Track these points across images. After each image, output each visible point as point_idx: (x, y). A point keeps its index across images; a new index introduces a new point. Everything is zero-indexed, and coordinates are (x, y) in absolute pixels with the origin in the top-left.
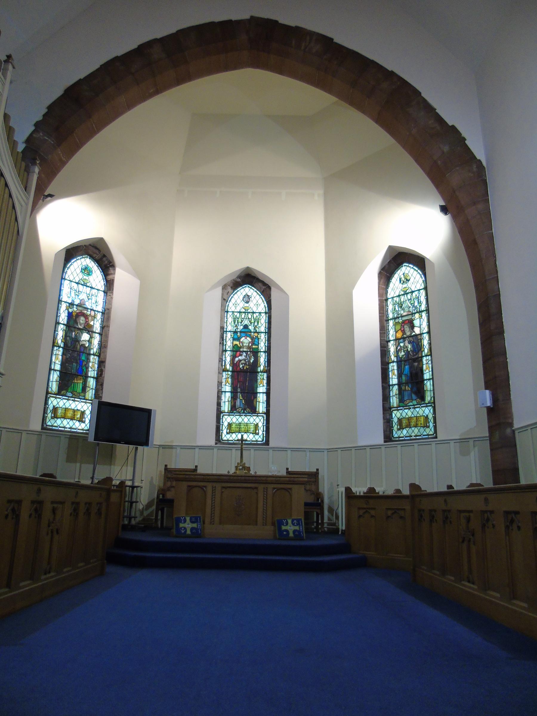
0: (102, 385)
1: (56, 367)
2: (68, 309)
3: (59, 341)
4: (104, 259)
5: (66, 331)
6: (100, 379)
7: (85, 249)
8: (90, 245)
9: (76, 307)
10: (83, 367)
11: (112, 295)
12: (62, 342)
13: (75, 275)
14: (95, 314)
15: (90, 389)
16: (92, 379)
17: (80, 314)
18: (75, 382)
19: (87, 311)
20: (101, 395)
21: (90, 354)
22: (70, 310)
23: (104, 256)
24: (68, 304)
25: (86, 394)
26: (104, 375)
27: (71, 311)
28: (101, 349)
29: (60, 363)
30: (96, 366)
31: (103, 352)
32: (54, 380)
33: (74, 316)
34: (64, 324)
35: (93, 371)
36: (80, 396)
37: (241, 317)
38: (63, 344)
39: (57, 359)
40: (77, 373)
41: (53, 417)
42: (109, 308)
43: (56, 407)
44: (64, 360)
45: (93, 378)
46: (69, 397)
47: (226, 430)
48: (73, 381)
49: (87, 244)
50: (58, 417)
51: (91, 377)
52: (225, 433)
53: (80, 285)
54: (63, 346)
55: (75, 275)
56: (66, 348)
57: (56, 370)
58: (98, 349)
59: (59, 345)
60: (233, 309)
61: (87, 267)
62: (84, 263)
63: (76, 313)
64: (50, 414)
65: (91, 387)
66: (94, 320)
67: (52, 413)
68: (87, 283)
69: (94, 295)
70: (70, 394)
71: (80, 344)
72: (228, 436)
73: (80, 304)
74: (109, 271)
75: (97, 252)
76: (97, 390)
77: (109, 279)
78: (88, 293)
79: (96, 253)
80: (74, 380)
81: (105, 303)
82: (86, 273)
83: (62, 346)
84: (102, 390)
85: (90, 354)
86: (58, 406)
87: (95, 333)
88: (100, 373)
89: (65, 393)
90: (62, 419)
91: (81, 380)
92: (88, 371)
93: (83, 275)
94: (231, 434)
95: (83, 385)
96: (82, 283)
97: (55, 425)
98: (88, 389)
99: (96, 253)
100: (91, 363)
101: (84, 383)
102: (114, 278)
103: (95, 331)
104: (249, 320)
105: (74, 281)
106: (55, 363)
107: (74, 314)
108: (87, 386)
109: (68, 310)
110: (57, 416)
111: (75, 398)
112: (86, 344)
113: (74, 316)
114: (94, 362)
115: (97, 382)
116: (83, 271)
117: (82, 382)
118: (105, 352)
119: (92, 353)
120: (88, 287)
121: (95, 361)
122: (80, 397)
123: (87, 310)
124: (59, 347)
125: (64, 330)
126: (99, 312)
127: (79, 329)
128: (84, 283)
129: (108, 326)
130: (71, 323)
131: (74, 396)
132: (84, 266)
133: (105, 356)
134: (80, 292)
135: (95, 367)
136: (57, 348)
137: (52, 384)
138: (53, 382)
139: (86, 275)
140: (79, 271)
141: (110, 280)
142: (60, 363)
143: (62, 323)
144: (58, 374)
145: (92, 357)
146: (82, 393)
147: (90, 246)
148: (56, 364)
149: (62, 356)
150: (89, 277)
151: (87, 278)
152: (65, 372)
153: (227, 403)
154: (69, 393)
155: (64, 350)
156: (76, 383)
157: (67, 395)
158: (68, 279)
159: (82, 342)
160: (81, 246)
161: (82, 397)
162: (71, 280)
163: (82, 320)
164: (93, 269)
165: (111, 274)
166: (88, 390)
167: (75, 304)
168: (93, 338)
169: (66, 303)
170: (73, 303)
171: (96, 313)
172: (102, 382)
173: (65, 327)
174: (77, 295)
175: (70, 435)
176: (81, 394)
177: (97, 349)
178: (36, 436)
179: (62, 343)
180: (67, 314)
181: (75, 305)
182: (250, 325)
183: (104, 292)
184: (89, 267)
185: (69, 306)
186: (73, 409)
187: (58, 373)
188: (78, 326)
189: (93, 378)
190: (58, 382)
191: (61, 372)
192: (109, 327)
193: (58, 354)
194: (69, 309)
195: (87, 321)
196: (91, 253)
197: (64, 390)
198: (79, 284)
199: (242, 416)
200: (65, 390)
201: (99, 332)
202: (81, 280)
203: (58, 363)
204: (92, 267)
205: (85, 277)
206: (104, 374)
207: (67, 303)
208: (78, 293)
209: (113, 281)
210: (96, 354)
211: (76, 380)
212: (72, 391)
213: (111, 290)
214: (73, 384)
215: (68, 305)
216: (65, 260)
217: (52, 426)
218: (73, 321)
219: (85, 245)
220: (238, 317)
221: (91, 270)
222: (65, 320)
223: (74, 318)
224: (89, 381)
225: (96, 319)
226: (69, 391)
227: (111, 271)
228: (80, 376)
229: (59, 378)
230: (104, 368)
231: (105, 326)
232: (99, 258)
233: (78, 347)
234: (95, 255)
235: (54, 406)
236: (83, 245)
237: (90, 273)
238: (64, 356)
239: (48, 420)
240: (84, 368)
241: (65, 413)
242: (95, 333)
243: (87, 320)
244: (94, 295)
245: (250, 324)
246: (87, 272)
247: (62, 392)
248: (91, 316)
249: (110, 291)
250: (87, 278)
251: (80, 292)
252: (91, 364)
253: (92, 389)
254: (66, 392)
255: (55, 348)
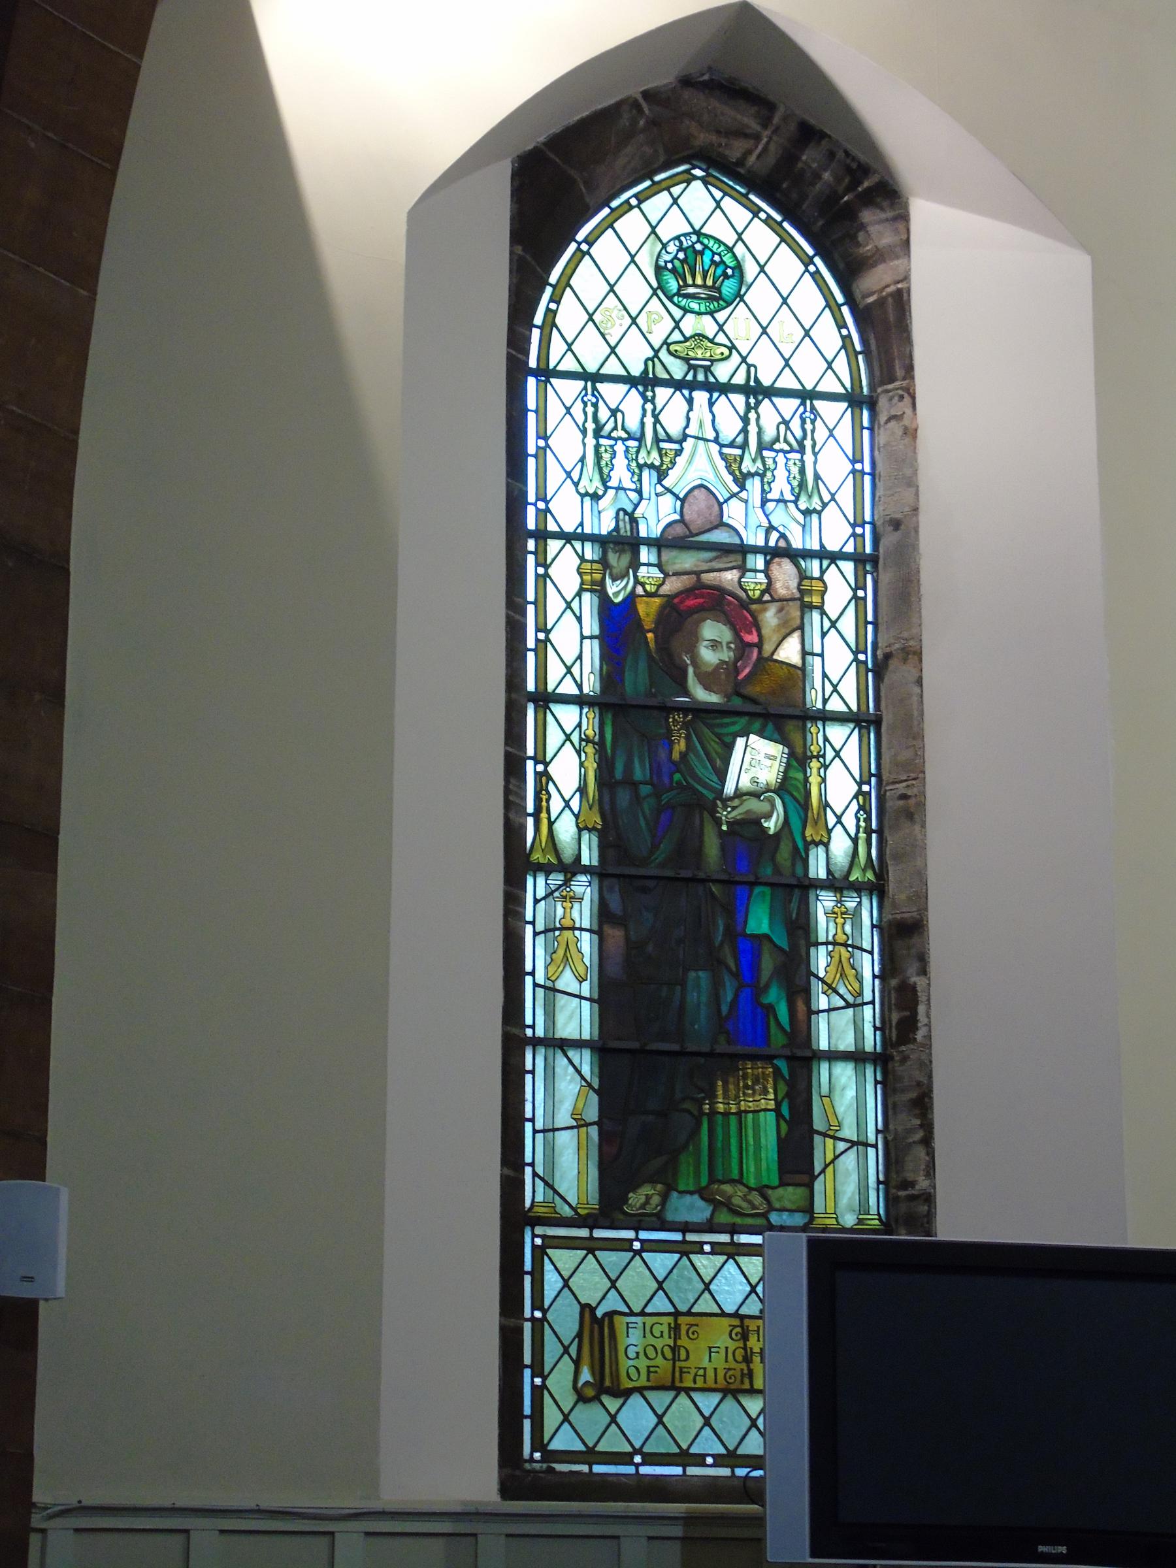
0: (922, 1104)
1: (561, 1019)
2: (593, 583)
3: (557, 826)
4: (810, 157)
5: (600, 745)
6: (905, 1059)
7: (653, 123)
8: (686, 82)
9: (653, 559)
10: (767, 987)
11: (909, 411)
12: (580, 830)
13: (616, 326)
14: (803, 576)
15: (842, 1146)
16: (845, 1073)
17: (690, 602)
18: (721, 1107)
19: (743, 569)
20: (923, 1183)
21: (808, 886)
22: (616, 590)
23: (808, 134)
24: (588, 546)
25: (818, 1186)
26: (928, 1025)
27: (616, 594)
28: (887, 833)
29: (586, 986)
30: (868, 966)
31: (897, 857)
32: (564, 1118)
33: (648, 623)
34: (580, 700)
35: (848, 1005)
36: (771, 1209)
37: (657, 420)
38: (595, 840)
39: (566, 959)
40: (722, 1047)
41: (590, 1393)
42: (898, 516)
43: (606, 1314)
44: (614, 970)
45: (857, 1057)
46: (685, 1228)
47: (573, 1366)
48: (700, 1103)
49: (663, 79)
50: (627, 1384)
51: (834, 1056)
52: (567, 1402)
53: (662, 393)
54: (595, 863)
55: (616, 326)
56: (618, 871)
57: (564, 1045)
58: (862, 835)
59: (568, 855)
60: (591, 354)
61: (698, 247)
62: (672, 226)
63: (657, 600)
64: (567, 1365)
65: (849, 1132)
66: (801, 628)
67: (577, 1363)
68: (712, 362)
69: (777, 440)
70: (691, 1207)
71: (718, 823)
72: (590, 1418)
73: (679, 530)
74: (861, 236)
75: (748, 119)
76: (891, 1145)
77: (871, 300)
78: (728, 434)
79: (741, 133)
80: (712, 1096)
81: (867, 479)
82: (691, 290)
83: (589, 857)
84: (927, 1141)
85: (808, 886)
86: (612, 1303)
87: (827, 717)
88: (895, 1017)
89: (656, 1200)
90: (660, 1399)
91: (765, 1092)
92: (811, 1012)
93: (678, 314)
94: (612, 1404)
95: (784, 1127)
96: (678, 370)
97: (612, 1443)
98: (823, 1150)
99: (741, 133)
100: (822, 949)
101: (785, 1110)
102: (906, 278)
103: (819, 705)
104: (726, 450)
105: (612, 368)
106: (551, 990)
107: (647, 610)
108: (818, 1124)
109: (598, 589)
110: (616, 1376)
111: (733, 1230)
112: (768, 816)
113: (648, 623)
114: (841, 938)
115: (887, 1085)
116: (673, 285)
117: (772, 1105)
118: (915, 851)
119: (822, 874)
120: (726, 389)
121: (848, 928)
122: (774, 1218)
123: (735, 559)
124: (572, 869)
125: (588, 740)
126: (834, 557)
127: (701, 712)
128: (691, 367)
129: (913, 653)
130: (636, 682)
131: (724, 1217)
132: (672, 248)
133: (921, 876)
134: (670, 439)
135: (859, 978)
136: (557, 879)
137: (550, 1151)
138: (554, 1130)
139: (694, 306)
140: (635, 290)
141: (881, 302)
142: (586, 990)
143: (569, 688)
144: (586, 1070)
145: (824, 903)
146: (782, 1184)
147: (687, 94)
148: (562, 1000)
149: (598, 931)
150: (721, 316)
151: (708, 326)
152: (634, 1045)
153: (567, 1141)
154: (688, 1199)
155: (606, 883)
156: (726, 1114)
157: (670, 1216)
158: (569, 364)
159: (736, 802)
160: (618, 105)
161: (785, 1215)
162: (592, 368)
163: (715, 645)
164: (740, 250)
165: (880, 256)
166: (830, 1157)
167: (643, 533)
168: (814, 764)
169: (578, 545)
170: (626, 528)
171: (814, 567)
172: (919, 1084)
173: (590, 722)
174: (651, 466)
175: (689, 1520)
176: (781, 1191)
177: (855, 841)
178: (438, 1544)
179: (586, 836)
180: (591, 625)
181: (650, 542)
182: (734, 495)
183: (854, 399)
184: (711, 243)
185: (604, 562)
186: (736, 1315)
187: (585, 1061)
188: (686, 693)
189: (857, 1057)
190: (594, 1131)
191: (601, 1048)
192: (919, 654)
193: (567, 923)
194: (602, 583)
195: (751, 645)
196: (703, 138)
197: (638, 1186)
198: (657, 382)
199: (702, 1252)
200: (652, 1181)
201: (854, 708)
202: (663, 354)
203: (573, 987)
204: (729, 238)
205: (690, 325)
206: (928, 1016)
207: (584, 538)
208: (655, 454)
209: (901, 300)
210: (852, 878)
211: (726, 1095)
212: (704, 1181)
213: (900, 372)
214: (705, 1126)
215: (590, 551)
216: (519, 235)
217: (591, 1455)
218: (642, 665)
219: (646, 94)
220: (633, 425)
221: (728, 259)
222: (587, 668)
223: (650, 635)
224: (825, 1090)
225: (816, 615)
226: (686, 1181)
227: (872, 229)
228: (754, 1058)
229: (594, 1098)
230: (924, 971)
231: (888, 656)
232: (771, 160)
233: (712, 847)
234: (735, 150)
235: (587, 1310)
236: (635, 91)
237: (728, 288)
238: (616, 935)
239: (551, 1417)
240: (775, 996)
241: (675, 1349)
242: (827, 717)
243: (753, 638)
244: (777, 440)
245: (736, 489)
246: (704, 286)
247: (636, 1199)
248: (773, 600)
249: (892, 380)
250: (708, 326)
251: (670, 439)
252: (821, 961)
253: (860, 1144)
254: (665, 1198)
255: (536, 886)
